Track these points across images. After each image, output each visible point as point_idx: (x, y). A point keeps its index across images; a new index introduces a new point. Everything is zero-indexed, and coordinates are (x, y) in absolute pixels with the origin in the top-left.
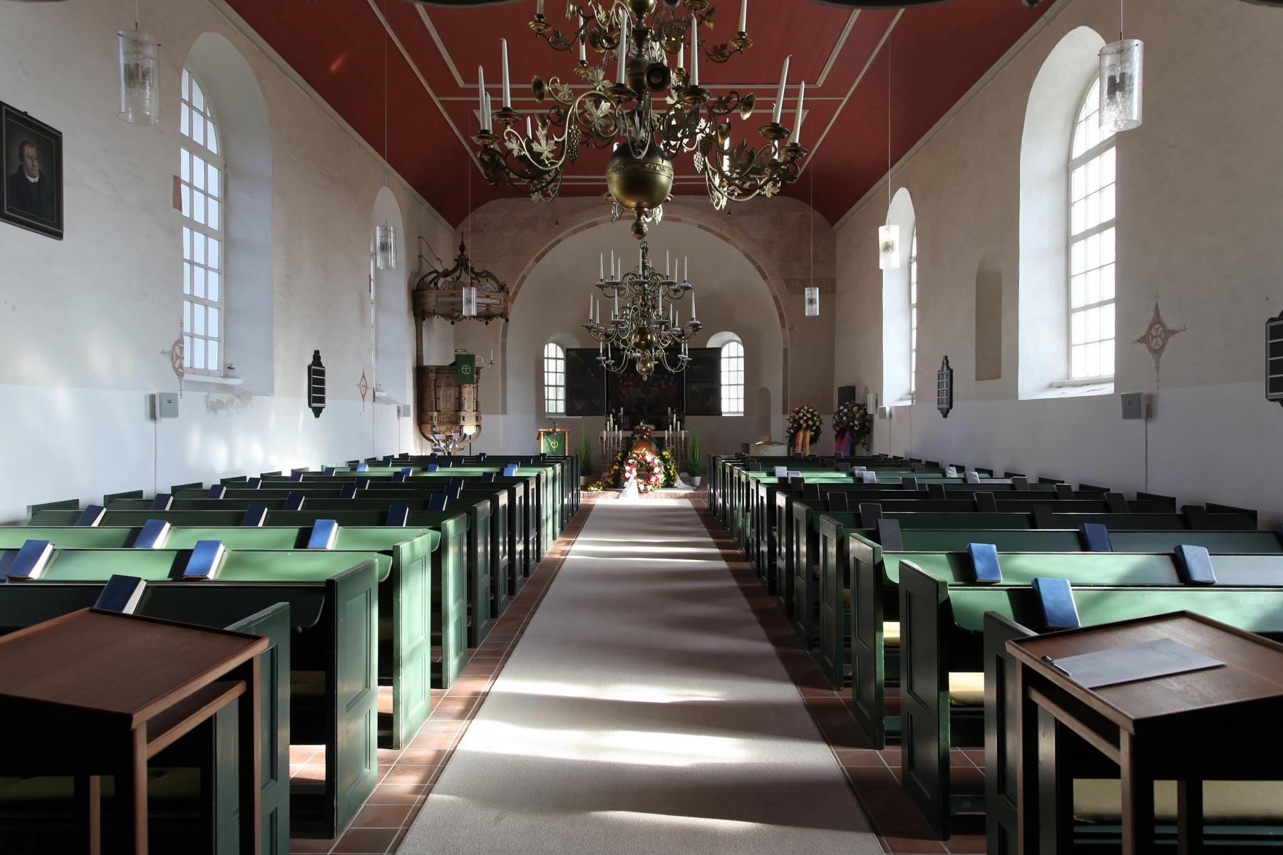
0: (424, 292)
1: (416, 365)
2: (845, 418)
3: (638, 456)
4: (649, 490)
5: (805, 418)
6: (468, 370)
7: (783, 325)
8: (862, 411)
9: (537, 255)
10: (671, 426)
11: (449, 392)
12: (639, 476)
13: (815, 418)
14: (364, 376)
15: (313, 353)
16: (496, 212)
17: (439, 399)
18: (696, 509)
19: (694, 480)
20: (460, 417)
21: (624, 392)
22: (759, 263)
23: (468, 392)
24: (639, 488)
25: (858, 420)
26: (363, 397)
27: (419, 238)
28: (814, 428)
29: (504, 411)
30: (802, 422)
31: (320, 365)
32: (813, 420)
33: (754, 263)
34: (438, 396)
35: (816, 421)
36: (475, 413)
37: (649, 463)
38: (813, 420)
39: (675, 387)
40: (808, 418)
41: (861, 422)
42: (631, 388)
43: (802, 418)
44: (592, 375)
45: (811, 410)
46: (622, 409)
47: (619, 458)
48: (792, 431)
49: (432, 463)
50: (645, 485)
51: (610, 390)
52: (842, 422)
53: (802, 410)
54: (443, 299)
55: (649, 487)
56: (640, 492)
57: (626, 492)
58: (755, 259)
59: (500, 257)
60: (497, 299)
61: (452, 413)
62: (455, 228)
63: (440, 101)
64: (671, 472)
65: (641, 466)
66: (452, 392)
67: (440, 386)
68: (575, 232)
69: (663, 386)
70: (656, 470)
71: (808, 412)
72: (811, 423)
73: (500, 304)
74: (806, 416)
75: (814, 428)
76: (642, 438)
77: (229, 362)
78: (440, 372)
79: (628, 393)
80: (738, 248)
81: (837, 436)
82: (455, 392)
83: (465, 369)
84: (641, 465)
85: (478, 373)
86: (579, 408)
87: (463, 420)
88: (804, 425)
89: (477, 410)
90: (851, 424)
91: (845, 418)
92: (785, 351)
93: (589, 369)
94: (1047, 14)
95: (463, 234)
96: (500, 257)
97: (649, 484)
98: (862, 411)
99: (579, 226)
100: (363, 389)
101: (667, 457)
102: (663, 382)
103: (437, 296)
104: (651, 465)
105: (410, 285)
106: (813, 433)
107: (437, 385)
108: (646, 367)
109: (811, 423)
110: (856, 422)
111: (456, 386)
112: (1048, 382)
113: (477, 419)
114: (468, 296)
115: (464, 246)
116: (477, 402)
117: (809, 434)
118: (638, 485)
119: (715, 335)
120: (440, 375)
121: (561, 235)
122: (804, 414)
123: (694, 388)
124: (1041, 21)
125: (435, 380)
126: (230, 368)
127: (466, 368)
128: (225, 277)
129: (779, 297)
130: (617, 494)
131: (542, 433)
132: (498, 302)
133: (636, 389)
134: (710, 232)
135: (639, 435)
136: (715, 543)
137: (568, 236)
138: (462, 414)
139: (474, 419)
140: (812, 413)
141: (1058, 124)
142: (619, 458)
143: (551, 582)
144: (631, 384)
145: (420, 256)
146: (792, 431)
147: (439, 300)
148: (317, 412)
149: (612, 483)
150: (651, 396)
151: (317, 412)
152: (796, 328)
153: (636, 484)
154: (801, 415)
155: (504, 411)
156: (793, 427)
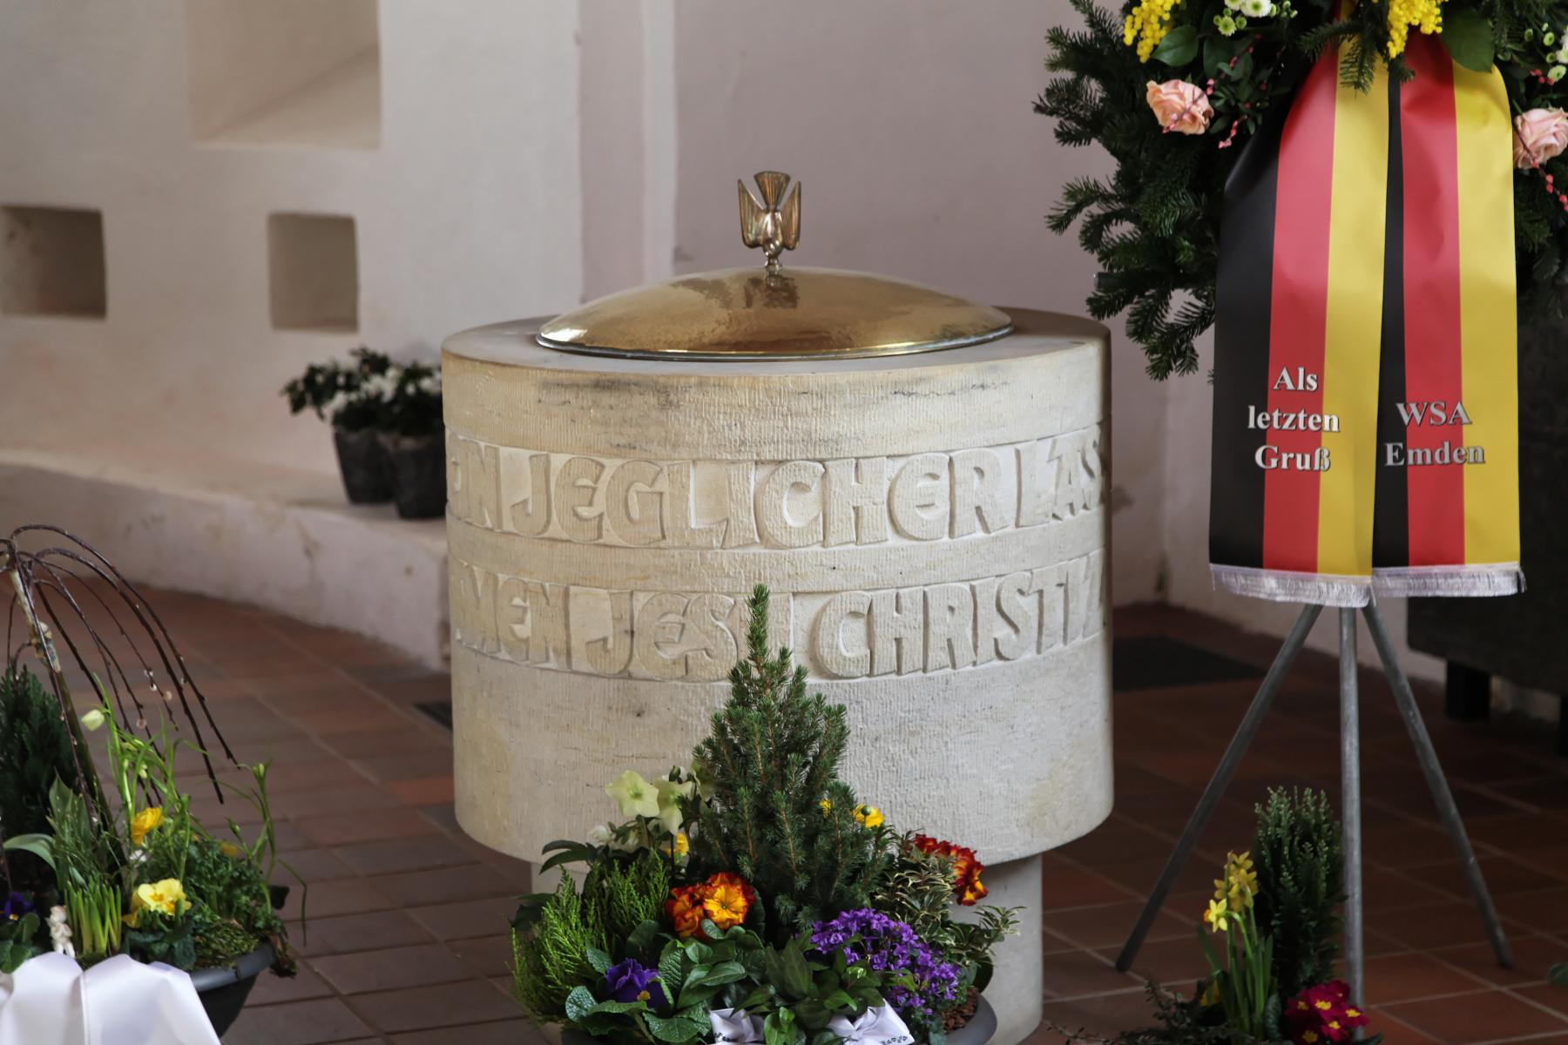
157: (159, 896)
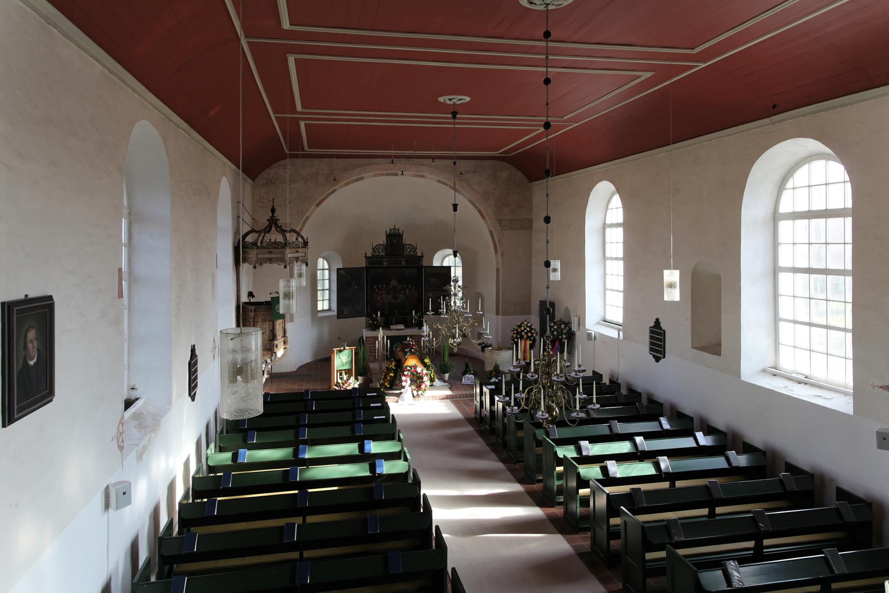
2: (555, 333)
3: (412, 369)
4: (420, 394)
7: (496, 252)
8: (567, 328)
13: (533, 331)
14: (214, 341)
16: (286, 169)
18: (470, 421)
19: (444, 377)
20: (273, 345)
21: (379, 298)
22: (480, 208)
24: (413, 394)
25: (565, 334)
30: (523, 333)
33: (476, 207)
37: (420, 373)
38: (531, 332)
39: (416, 294)
41: (567, 336)
42: (384, 296)
43: (523, 331)
44: (356, 287)
46: (379, 313)
47: (393, 367)
50: (417, 391)
53: (523, 325)
54: (262, 256)
55: (420, 392)
56: (414, 396)
57: (403, 396)
58: (477, 204)
62: (253, 181)
63: (276, 117)
64: (432, 375)
65: (413, 376)
67: (258, 322)
68: (347, 184)
69: (408, 293)
70: (425, 379)
71: (527, 326)
72: (530, 334)
74: (526, 329)
75: (532, 338)
77: (132, 384)
78: (257, 310)
79: (382, 299)
80: (465, 196)
82: (269, 326)
84: (414, 375)
86: (346, 312)
87: (276, 347)
88: (525, 336)
89: (284, 336)
90: (560, 337)
91: (555, 333)
92: (498, 270)
93: (353, 283)
94: (773, 118)
95: (273, 200)
98: (567, 328)
101: (428, 364)
102: (407, 291)
103: (257, 254)
106: (531, 342)
107: (255, 321)
109: (530, 334)
110: (564, 336)
112: (761, 367)
114: (299, 271)
115: (275, 209)
116: (284, 329)
117: (528, 342)
118: (412, 391)
119: (441, 251)
120: (257, 313)
121: (336, 187)
124: (767, 120)
125: (254, 317)
126: (133, 389)
128: (129, 310)
130: (396, 398)
131: (335, 351)
133: (388, 296)
134: (445, 185)
136: (530, 493)
138: (276, 342)
140: (530, 327)
141: (770, 188)
142: (393, 367)
144: (384, 292)
145: (238, 217)
147: (259, 256)
148: (193, 400)
149: (388, 386)
150: (399, 300)
151: (193, 400)
152: (506, 254)
153: (411, 390)
154: (522, 328)
157: (472, 372)
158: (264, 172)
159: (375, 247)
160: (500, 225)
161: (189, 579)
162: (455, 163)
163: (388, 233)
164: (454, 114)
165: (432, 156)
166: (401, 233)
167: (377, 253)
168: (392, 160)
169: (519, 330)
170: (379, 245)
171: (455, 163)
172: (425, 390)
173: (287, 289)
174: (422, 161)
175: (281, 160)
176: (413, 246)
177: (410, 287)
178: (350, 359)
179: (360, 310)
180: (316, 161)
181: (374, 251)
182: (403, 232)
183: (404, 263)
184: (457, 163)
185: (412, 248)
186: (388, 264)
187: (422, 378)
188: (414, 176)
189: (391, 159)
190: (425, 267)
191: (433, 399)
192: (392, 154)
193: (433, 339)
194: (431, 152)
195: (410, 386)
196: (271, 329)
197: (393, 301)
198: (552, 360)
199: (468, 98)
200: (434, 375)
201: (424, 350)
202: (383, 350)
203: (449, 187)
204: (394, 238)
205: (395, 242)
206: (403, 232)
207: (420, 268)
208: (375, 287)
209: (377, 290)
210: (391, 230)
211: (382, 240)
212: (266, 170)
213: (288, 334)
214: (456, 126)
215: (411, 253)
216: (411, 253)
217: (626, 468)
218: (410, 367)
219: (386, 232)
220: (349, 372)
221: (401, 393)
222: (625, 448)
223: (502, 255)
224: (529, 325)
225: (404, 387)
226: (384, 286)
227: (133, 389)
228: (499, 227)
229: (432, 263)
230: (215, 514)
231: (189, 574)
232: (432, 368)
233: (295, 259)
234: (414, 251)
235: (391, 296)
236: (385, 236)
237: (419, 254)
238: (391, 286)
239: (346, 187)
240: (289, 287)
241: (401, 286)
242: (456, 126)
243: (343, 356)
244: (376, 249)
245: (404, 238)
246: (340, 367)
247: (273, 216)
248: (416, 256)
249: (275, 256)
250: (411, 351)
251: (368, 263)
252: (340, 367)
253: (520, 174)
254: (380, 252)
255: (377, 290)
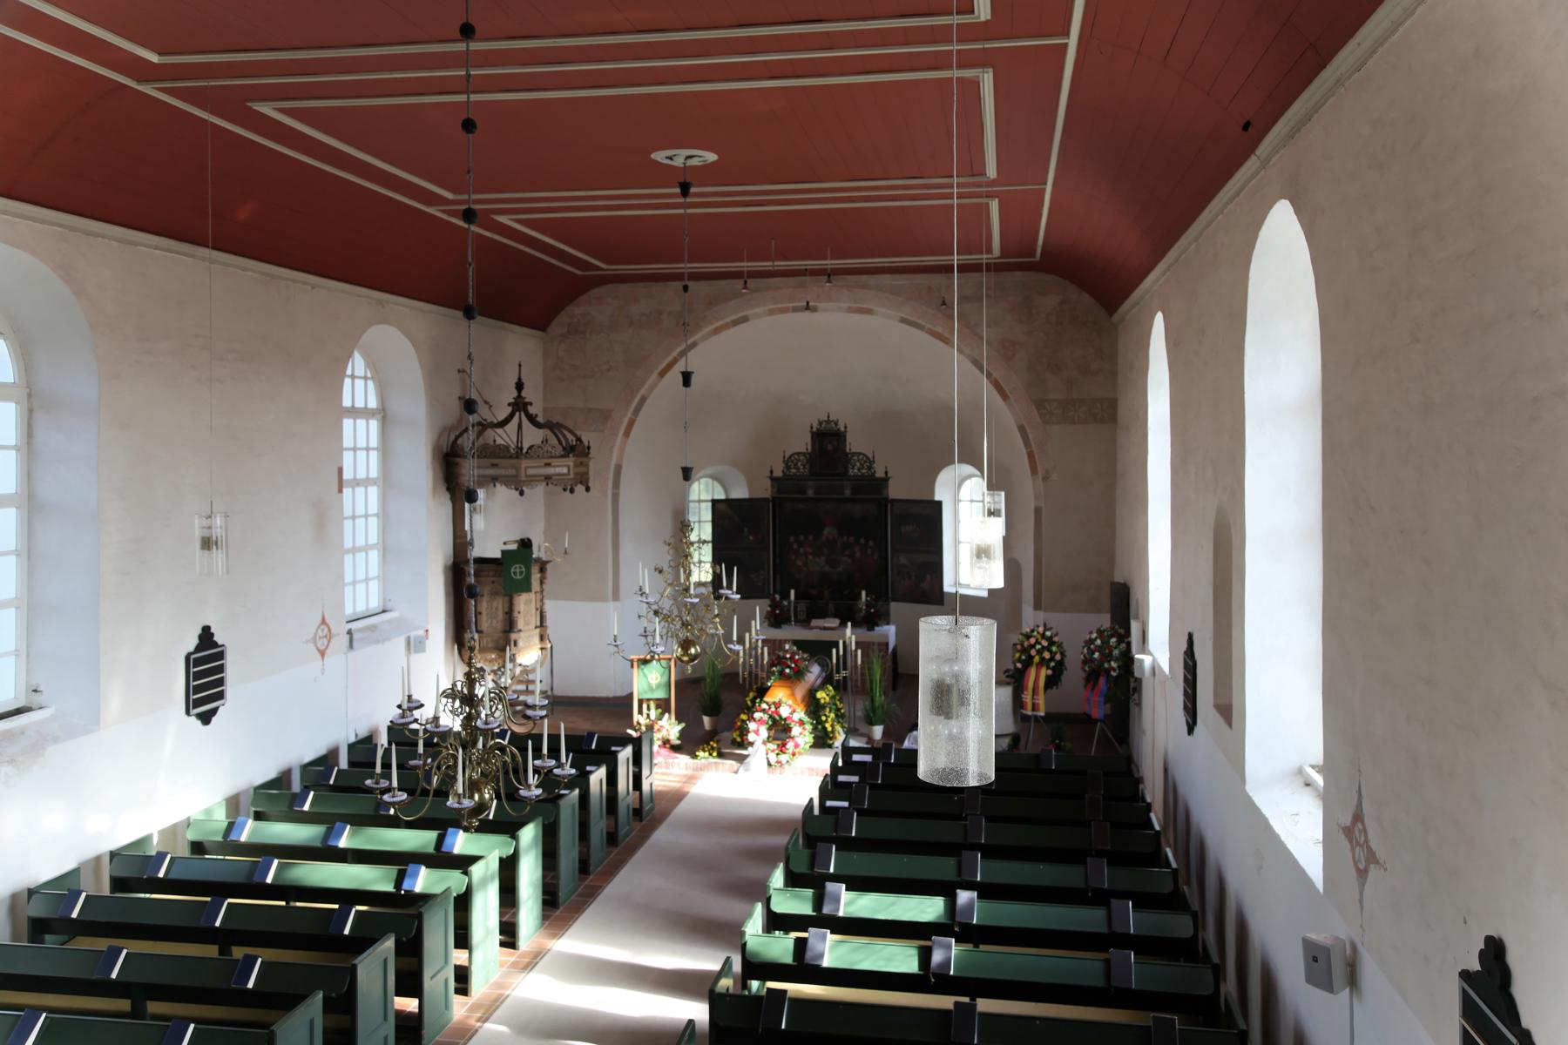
0: (458, 460)
1: (452, 560)
5: (1038, 647)
6: (521, 573)
8: (1123, 646)
9: (661, 367)
10: (834, 651)
11: (495, 604)
12: (769, 739)
13: (1054, 649)
14: (324, 622)
15: (199, 631)
17: (480, 613)
21: (800, 563)
23: (525, 604)
25: (1116, 660)
26: (322, 654)
27: (459, 371)
28: (1052, 664)
29: (616, 596)
30: (1033, 652)
31: (215, 645)
32: (1051, 652)
34: (479, 610)
35: (1056, 653)
36: (538, 630)
37: (785, 719)
38: (1051, 652)
39: (876, 557)
40: (1043, 647)
42: (811, 557)
43: (1033, 646)
44: (751, 538)
45: (1048, 634)
46: (792, 592)
48: (1019, 665)
49: (341, 821)
50: (778, 754)
51: (778, 561)
52: (1092, 660)
53: (1035, 633)
55: (783, 758)
56: (769, 764)
59: (609, 370)
60: (565, 466)
61: (501, 635)
64: (828, 725)
66: (500, 604)
67: (482, 596)
68: (717, 331)
69: (858, 555)
70: (796, 730)
71: (1043, 636)
72: (1047, 655)
73: (569, 474)
74: (1040, 644)
75: (1052, 664)
76: (782, 673)
81: (1087, 680)
83: (517, 571)
85: (542, 570)
88: (1037, 659)
90: (1106, 665)
91: (1096, 655)
92: (1038, 511)
93: (746, 529)
95: (520, 366)
96: (609, 370)
97: (784, 753)
99: (721, 323)
100: (322, 643)
101: (822, 701)
102: (857, 549)
104: (788, 722)
105: (437, 448)
106: (1050, 672)
108: (688, 655)
109: (1047, 655)
110: (1113, 664)
111: (505, 595)
113: (542, 638)
117: (1044, 672)
122: (1037, 640)
123: (903, 560)
124: (1251, 164)
126: (35, 691)
127: (518, 570)
128: (29, 558)
129: (1026, 426)
132: (565, 470)
133: (817, 560)
135: (779, 668)
137: (706, 337)
138: (513, 636)
139: (537, 639)
140: (1050, 640)
143: (470, 1038)
144: (810, 550)
146: (1019, 665)
150: (840, 569)
152: (1054, 477)
154: (1032, 641)
155: (616, 596)
156: (1019, 660)
158: (563, 313)
159: (790, 457)
160: (1041, 415)
161: (52, 1019)
162: (686, 289)
163: (814, 429)
164: (685, 189)
165: (826, 269)
166: (843, 429)
167: (794, 471)
168: (745, 282)
169: (1026, 644)
170: (798, 454)
171: (686, 289)
172: (794, 754)
173: (205, 531)
174: (864, 278)
175: (593, 288)
176: (867, 458)
177: (862, 541)
178: (665, 679)
179: (760, 584)
180: (657, 288)
181: (788, 467)
182: (846, 427)
183: (848, 492)
184: (690, 288)
185: (866, 462)
186: (815, 493)
187: (790, 729)
188: (851, 310)
189: (683, 283)
190: (893, 501)
191: (810, 775)
192: (829, 267)
193: (856, 650)
194: (742, 264)
195: (764, 743)
196: (506, 610)
197: (827, 568)
198: (749, 702)
199: (713, 154)
200: (832, 726)
201: (838, 672)
202: (756, 667)
203: (927, 332)
204: (828, 440)
205: (830, 447)
206: (846, 427)
207: (884, 502)
208: (792, 539)
209: (795, 546)
210: (820, 423)
211: (801, 443)
212: (568, 308)
213: (549, 622)
214: (689, 211)
215: (863, 471)
216: (863, 471)
217: (855, 950)
218: (767, 703)
219: (812, 428)
220: (663, 705)
221: (746, 756)
222: (930, 910)
223: (1045, 479)
224: (1048, 634)
225: (751, 744)
226: (811, 538)
227: (35, 691)
228: (1038, 419)
229: (932, 492)
230: (346, 932)
231: (50, 1010)
232: (830, 711)
233: (543, 478)
234: (870, 468)
235: (823, 558)
236: (809, 435)
237: (880, 474)
238: (824, 539)
239: (717, 336)
240: (210, 528)
241: (845, 538)
242: (689, 211)
243: (651, 672)
244: (792, 462)
245: (849, 439)
246: (646, 692)
247: (519, 396)
248: (872, 478)
249: (502, 472)
250: (782, 673)
251: (775, 490)
252: (646, 692)
253: (1086, 297)
254: (798, 469)
255: (795, 546)
